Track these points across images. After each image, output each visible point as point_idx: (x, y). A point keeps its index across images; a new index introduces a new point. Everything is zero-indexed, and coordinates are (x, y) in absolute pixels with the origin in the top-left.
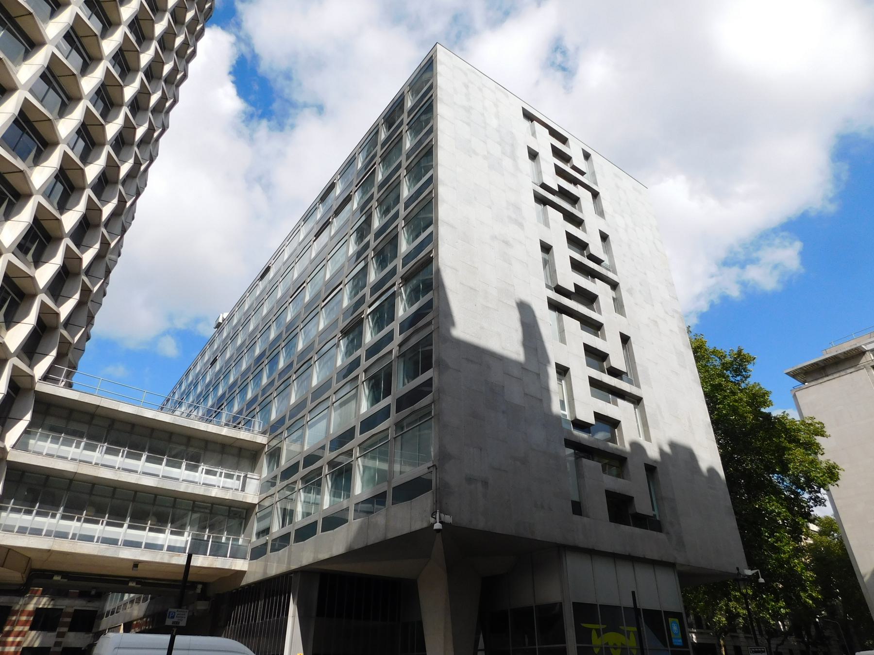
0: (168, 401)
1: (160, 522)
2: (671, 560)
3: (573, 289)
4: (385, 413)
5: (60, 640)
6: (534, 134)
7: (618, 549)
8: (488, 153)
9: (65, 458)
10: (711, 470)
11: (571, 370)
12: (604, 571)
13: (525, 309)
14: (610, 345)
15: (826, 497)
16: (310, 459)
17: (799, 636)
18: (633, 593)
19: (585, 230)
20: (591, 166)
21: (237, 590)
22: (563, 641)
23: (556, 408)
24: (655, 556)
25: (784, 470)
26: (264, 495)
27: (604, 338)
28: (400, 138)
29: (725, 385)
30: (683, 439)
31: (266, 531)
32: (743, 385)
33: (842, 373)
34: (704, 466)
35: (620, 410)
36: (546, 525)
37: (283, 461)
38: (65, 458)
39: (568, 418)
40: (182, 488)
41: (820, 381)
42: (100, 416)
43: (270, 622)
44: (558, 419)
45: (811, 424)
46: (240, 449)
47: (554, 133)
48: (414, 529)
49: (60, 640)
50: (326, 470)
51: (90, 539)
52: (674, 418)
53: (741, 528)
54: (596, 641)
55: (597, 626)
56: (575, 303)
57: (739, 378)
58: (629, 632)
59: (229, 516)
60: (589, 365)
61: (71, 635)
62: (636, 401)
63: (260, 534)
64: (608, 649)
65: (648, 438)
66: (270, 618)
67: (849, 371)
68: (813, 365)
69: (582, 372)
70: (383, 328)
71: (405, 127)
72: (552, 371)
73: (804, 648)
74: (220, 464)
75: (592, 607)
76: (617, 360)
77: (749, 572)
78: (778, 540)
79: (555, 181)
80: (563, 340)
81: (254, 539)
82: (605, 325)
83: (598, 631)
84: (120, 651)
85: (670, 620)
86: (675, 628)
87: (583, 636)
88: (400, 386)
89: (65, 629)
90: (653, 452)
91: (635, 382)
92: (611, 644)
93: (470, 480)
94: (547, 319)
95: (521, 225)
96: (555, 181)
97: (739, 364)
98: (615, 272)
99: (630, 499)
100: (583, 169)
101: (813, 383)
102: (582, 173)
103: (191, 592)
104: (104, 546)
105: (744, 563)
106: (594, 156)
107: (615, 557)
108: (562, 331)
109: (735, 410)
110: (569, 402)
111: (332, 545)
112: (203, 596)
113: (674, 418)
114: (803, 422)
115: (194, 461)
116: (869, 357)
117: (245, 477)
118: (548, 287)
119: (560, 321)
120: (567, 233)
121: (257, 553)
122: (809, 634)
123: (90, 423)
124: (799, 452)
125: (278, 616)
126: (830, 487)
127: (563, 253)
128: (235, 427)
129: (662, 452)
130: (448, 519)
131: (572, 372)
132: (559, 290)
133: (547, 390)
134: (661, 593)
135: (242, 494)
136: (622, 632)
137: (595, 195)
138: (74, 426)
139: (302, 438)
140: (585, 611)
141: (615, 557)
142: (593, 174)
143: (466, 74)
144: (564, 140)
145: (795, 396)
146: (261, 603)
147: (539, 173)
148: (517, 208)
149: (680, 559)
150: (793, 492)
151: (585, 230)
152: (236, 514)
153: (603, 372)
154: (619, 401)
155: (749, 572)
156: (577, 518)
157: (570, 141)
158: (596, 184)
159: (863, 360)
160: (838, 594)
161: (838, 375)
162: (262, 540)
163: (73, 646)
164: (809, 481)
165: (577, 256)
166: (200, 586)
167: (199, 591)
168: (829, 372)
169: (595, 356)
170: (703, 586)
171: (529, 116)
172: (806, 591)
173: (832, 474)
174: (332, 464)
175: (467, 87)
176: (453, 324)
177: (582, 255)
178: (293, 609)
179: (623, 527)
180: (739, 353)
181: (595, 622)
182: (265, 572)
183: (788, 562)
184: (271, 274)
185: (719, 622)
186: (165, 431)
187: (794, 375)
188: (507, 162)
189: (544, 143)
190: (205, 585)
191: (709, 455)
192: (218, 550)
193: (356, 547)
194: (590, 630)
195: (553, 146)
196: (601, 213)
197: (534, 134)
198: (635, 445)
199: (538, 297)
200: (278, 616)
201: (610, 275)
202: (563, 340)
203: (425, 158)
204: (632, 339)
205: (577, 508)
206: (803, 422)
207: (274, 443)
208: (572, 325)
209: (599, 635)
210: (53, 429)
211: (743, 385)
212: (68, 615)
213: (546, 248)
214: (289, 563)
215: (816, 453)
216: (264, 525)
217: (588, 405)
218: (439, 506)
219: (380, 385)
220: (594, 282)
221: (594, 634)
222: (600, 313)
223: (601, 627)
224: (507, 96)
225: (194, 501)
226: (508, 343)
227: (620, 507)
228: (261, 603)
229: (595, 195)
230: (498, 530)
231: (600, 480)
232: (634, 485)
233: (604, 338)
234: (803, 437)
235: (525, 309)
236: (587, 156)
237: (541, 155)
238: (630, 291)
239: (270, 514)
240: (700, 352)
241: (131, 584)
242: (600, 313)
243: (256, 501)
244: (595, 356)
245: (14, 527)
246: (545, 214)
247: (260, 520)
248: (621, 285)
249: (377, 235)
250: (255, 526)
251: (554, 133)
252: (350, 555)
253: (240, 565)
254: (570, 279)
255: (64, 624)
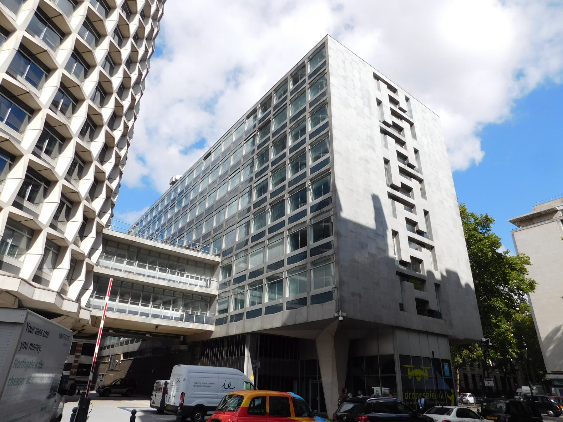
0: (137, 224)
1: (166, 304)
2: (446, 334)
3: (400, 186)
4: (303, 256)
5: (77, 359)
6: (379, 89)
7: (420, 328)
8: (356, 105)
9: (144, 275)
10: (467, 285)
11: (399, 233)
12: (414, 339)
13: (375, 199)
14: (419, 217)
15: (527, 298)
16: (254, 274)
17: (501, 369)
18: (433, 352)
19: (406, 149)
20: (409, 106)
21: (207, 341)
22: (394, 373)
23: (391, 253)
24: (438, 332)
25: (506, 282)
26: (222, 291)
27: (415, 213)
28: (303, 93)
29: (477, 234)
30: (453, 268)
31: (226, 310)
32: (486, 235)
33: (542, 223)
34: (463, 282)
35: (423, 254)
36: (388, 317)
37: (234, 273)
38: (144, 275)
39: (397, 259)
40: (181, 286)
41: (529, 227)
42: (133, 246)
43: (232, 359)
44: (393, 260)
45: (522, 258)
46: (205, 264)
47: (390, 87)
48: (325, 318)
49: (77, 359)
50: (265, 282)
51: (136, 313)
52: (450, 258)
53: (481, 314)
54: (410, 373)
55: (410, 366)
56: (401, 194)
57: (484, 231)
58: (425, 369)
59: (201, 301)
60: (408, 229)
61: (83, 357)
62: (431, 248)
63: (221, 312)
64: (415, 377)
65: (436, 269)
66: (232, 356)
67: (547, 222)
68: (525, 217)
69: (405, 233)
70: (298, 208)
71: (306, 85)
72: (389, 234)
73: (503, 375)
74: (195, 272)
75: (408, 357)
76: (422, 226)
77: (484, 340)
78: (499, 321)
79: (390, 119)
80: (395, 216)
81: (217, 314)
82: (416, 206)
83: (410, 368)
84: (191, 373)
85: (444, 363)
86: (446, 367)
87: (404, 371)
88: (312, 243)
89: (79, 354)
90: (438, 276)
91: (430, 238)
92: (416, 375)
93: (353, 294)
94: (386, 203)
95: (374, 149)
96: (390, 119)
97: (486, 222)
98: (421, 173)
99: (426, 302)
100: (405, 109)
101: (525, 228)
102: (404, 111)
103: (177, 340)
104: (144, 317)
105: (482, 335)
106: (411, 100)
107: (419, 332)
108: (394, 211)
109: (482, 251)
110: (398, 251)
111: (275, 321)
112: (184, 342)
113: (450, 258)
114: (518, 257)
115: (182, 271)
116: (560, 214)
117: (210, 280)
118: (388, 185)
119: (393, 205)
120: (398, 152)
121: (219, 322)
122: (506, 368)
123: (118, 247)
124: (514, 273)
125: (238, 356)
126: (530, 293)
127: (395, 164)
128: (193, 250)
129: (442, 276)
130: (345, 314)
131: (400, 234)
132: (393, 187)
133: (386, 245)
134: (442, 350)
135: (208, 289)
136: (421, 369)
137: (412, 124)
138: (120, 251)
139: (246, 261)
140: (405, 359)
141: (419, 332)
142: (411, 111)
143: (343, 54)
144: (394, 90)
145: (513, 235)
146: (225, 349)
147: (382, 114)
148: (372, 138)
149: (450, 333)
150: (509, 295)
151: (406, 149)
152: (206, 300)
153: (414, 232)
154: (423, 249)
155: (484, 340)
156: (402, 312)
157: (398, 91)
158: (412, 117)
159: (556, 216)
160: (526, 347)
161: (540, 224)
162: (223, 315)
163: (84, 363)
164: (519, 289)
165: (403, 166)
166: (182, 337)
167: (182, 339)
168: (534, 221)
169: (411, 224)
170: (458, 344)
171: (377, 77)
172: (512, 348)
173: (531, 286)
174: (269, 279)
175: (344, 62)
176: (340, 209)
177: (404, 164)
178: (247, 353)
179: (424, 317)
180: (486, 217)
181: (409, 364)
182: (227, 332)
183: (503, 333)
184: (212, 158)
185: (458, 361)
186: (166, 254)
187: (514, 222)
188: (366, 110)
189: (385, 93)
190: (184, 336)
191: (466, 277)
192: (199, 320)
193: (289, 324)
194: (407, 368)
195: (389, 96)
196: (414, 136)
197: (379, 89)
198: (430, 273)
199: (383, 191)
200: (238, 356)
201: (419, 175)
202: (395, 216)
203: (321, 109)
204: (430, 213)
205: (402, 307)
206: (518, 257)
207: (226, 262)
208: (400, 206)
209: (411, 371)
210: (119, 255)
211: (486, 235)
212: (80, 346)
213: (386, 162)
214: (244, 328)
215: (524, 274)
216: (224, 307)
217: (407, 253)
218: (340, 307)
219: (299, 240)
220: (411, 180)
221: (409, 370)
222: (414, 199)
223: (412, 366)
224: (365, 65)
225: (183, 293)
226: (367, 220)
227: (422, 306)
228: (225, 349)
229: (412, 124)
230: (366, 320)
231: (411, 293)
232: (428, 294)
233: (415, 213)
234: (518, 267)
235: (375, 199)
236: (407, 99)
237: (383, 103)
238: (429, 184)
239: (228, 301)
240: (463, 214)
241: (147, 335)
242: (414, 199)
243: (217, 294)
244: (411, 224)
245: (126, 310)
246: (386, 141)
247: (219, 304)
248: (425, 181)
249: (274, 134)
250: (217, 307)
251: (390, 87)
252: (284, 327)
253: (211, 328)
254: (399, 179)
255: (78, 351)
